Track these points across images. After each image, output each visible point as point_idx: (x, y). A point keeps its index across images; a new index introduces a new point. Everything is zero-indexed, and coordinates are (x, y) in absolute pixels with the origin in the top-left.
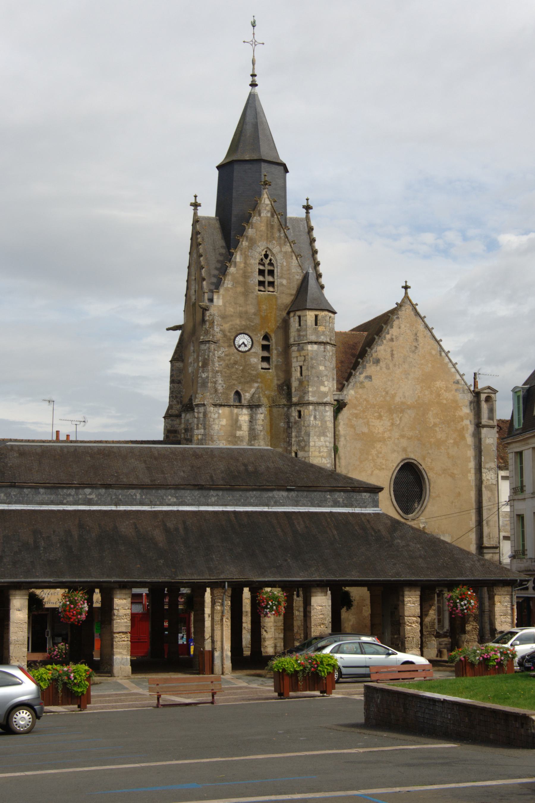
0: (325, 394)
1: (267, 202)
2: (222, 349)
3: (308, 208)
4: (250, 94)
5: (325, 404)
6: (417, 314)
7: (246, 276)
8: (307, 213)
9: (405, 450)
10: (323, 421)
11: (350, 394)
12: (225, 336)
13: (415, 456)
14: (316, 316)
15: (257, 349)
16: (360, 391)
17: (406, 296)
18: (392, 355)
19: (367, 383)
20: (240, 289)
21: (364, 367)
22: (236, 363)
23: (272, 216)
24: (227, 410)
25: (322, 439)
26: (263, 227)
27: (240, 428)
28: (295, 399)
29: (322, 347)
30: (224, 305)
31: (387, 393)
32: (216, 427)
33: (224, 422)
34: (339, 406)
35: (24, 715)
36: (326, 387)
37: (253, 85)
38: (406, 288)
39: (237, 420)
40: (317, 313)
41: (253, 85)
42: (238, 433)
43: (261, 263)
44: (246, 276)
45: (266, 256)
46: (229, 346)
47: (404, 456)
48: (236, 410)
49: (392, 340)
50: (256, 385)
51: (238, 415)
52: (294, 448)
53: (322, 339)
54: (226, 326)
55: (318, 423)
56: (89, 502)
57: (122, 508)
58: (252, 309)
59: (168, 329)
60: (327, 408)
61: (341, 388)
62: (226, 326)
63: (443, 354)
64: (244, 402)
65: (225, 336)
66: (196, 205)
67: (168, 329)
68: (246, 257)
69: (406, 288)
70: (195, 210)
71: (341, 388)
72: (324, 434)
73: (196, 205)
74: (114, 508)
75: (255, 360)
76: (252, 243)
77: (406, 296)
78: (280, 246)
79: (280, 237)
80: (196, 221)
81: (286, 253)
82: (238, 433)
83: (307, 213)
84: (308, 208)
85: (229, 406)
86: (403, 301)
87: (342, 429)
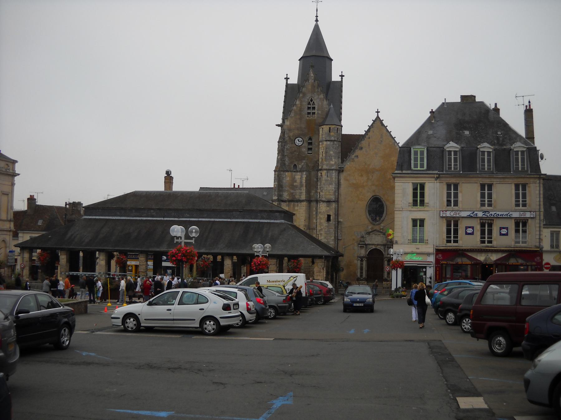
0: (332, 165)
1: (312, 75)
2: (289, 145)
3: (342, 76)
4: (315, 25)
5: (333, 170)
6: (383, 125)
7: (301, 110)
8: (342, 79)
9: (374, 191)
10: (331, 178)
11: (348, 165)
12: (290, 138)
13: (380, 194)
14: (330, 128)
15: (306, 144)
16: (352, 163)
17: (378, 117)
18: (369, 145)
19: (356, 159)
20: (298, 117)
21: (354, 151)
22: (295, 151)
23: (315, 81)
24: (290, 173)
25: (331, 186)
26: (310, 87)
27: (296, 181)
28: (320, 168)
29: (332, 143)
30: (290, 124)
31: (366, 164)
32: (284, 181)
33: (288, 179)
34: (340, 171)
35: (467, 326)
36: (334, 162)
37: (317, 21)
38: (378, 112)
39: (295, 178)
40: (330, 126)
41: (317, 21)
42: (295, 184)
43: (309, 104)
44: (301, 110)
45: (312, 100)
46: (292, 143)
47: (374, 194)
48: (294, 173)
49: (369, 138)
50: (304, 161)
51: (295, 175)
52: (319, 191)
53: (333, 138)
54: (291, 134)
55: (329, 179)
56: (153, 216)
57: (166, 219)
58: (303, 126)
59: (168, 173)
60: (334, 172)
61: (343, 161)
62: (291, 134)
63: (396, 144)
64: (298, 169)
65: (290, 138)
66: (287, 79)
67: (168, 173)
68: (301, 102)
69: (378, 112)
70: (287, 81)
71: (343, 161)
72: (331, 184)
73: (287, 79)
74: (162, 219)
75: (304, 150)
76: (304, 95)
77: (378, 117)
78: (318, 95)
79: (318, 91)
80: (287, 85)
81: (321, 98)
82: (295, 184)
83: (342, 79)
84: (342, 76)
85: (291, 171)
86: (376, 119)
87: (342, 181)
